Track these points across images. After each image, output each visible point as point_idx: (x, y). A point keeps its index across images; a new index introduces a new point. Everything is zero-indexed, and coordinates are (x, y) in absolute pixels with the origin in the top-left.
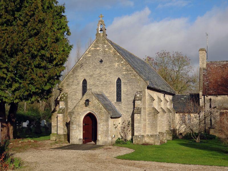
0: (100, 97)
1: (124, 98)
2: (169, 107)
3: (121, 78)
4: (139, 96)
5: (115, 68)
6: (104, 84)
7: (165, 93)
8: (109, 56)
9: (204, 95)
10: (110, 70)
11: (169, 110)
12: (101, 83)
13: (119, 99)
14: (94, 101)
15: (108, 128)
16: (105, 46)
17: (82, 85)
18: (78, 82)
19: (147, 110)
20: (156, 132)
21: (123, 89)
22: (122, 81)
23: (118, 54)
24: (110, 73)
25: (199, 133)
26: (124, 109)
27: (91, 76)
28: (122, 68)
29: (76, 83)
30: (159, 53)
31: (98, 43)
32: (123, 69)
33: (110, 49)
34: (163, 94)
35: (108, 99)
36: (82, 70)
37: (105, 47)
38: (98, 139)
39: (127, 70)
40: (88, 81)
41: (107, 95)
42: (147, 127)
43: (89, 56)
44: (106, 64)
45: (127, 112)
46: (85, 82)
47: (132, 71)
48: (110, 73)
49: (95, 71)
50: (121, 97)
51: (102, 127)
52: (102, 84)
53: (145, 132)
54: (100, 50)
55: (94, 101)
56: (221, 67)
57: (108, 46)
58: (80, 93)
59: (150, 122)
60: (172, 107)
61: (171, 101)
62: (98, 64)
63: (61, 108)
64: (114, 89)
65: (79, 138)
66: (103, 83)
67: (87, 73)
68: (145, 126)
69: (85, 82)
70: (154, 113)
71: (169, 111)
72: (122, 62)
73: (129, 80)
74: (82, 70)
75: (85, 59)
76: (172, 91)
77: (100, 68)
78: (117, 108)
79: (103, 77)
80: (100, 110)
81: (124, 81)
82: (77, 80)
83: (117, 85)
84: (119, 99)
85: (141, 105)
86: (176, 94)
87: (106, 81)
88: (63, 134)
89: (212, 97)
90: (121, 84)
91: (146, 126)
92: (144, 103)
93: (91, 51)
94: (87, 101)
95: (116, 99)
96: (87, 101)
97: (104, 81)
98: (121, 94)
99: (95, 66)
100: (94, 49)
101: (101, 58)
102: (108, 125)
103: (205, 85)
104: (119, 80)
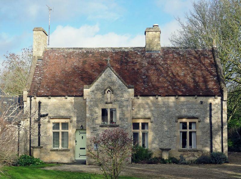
89: (43, 100)
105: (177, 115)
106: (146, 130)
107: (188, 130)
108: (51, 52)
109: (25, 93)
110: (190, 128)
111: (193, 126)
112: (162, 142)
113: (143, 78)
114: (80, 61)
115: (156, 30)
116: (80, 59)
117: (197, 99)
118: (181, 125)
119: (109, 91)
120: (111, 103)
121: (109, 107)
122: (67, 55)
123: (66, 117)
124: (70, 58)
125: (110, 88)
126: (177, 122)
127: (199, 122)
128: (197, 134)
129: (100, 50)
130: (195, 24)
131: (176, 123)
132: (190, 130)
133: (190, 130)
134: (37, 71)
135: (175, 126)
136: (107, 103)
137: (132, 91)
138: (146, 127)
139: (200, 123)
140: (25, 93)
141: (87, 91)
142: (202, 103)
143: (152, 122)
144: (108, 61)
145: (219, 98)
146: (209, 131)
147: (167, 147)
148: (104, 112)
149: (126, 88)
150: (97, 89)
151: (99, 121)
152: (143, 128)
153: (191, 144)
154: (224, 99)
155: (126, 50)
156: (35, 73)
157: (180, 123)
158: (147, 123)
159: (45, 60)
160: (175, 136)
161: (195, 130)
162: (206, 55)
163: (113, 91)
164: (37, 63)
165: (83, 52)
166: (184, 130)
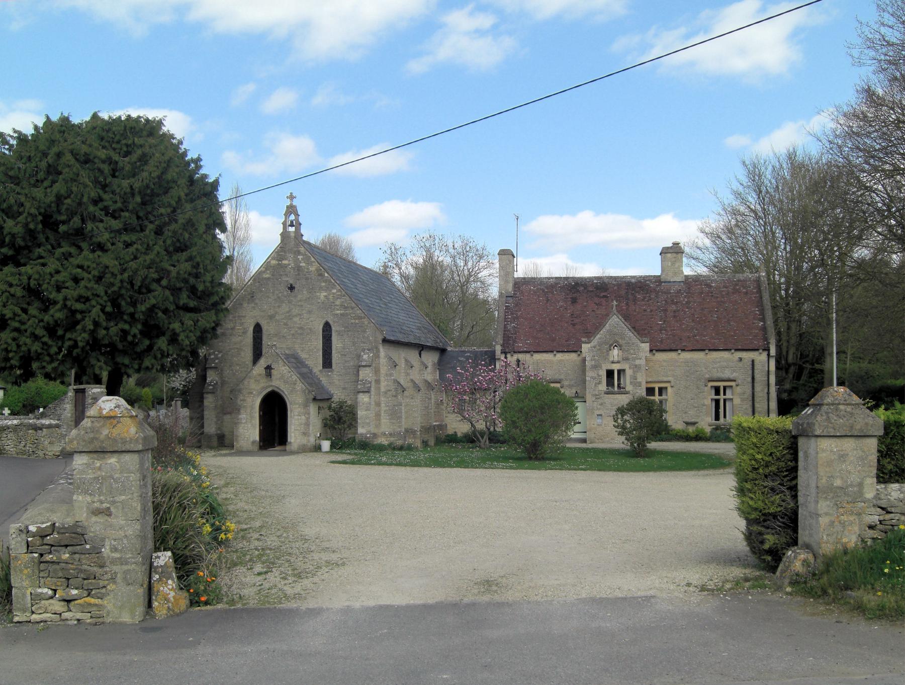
0: (295, 361)
1: (337, 362)
2: (429, 378)
3: (331, 323)
4: (367, 359)
5: (319, 303)
6: (298, 334)
7: (421, 348)
8: (307, 279)
9: (504, 352)
10: (309, 306)
11: (429, 383)
12: (292, 332)
13: (327, 362)
14: (282, 370)
15: (308, 419)
16: (300, 257)
17: (252, 336)
18: (244, 329)
19: (383, 385)
20: (400, 427)
21: (336, 343)
22: (333, 328)
23: (326, 275)
24: (310, 312)
25: (852, 552)
26: (337, 382)
27: (271, 317)
28: (334, 303)
29: (239, 331)
30: (417, 237)
31: (285, 252)
32: (336, 305)
33: (309, 263)
34: (417, 353)
35: (306, 363)
36: (253, 305)
37: (300, 259)
38: (289, 440)
39: (346, 308)
40: (265, 328)
41: (303, 355)
42: (382, 418)
43: (267, 276)
44: (302, 294)
45: (344, 389)
46: (258, 329)
47: (353, 308)
48: (310, 312)
49: (279, 307)
50: (331, 360)
51: (296, 417)
52: (293, 335)
53: (378, 426)
54: (289, 265)
55: (282, 370)
56: (543, 291)
57: (307, 259)
58: (249, 352)
59: (387, 408)
60: (438, 377)
61: (434, 364)
62: (285, 293)
63: (211, 382)
64: (319, 343)
65: (252, 440)
66: (297, 331)
67: (262, 311)
68: (378, 415)
69: (258, 329)
70: (396, 390)
71: (429, 386)
72: (334, 291)
73: (346, 327)
74: (253, 305)
75: (259, 282)
76: (441, 342)
77: (290, 302)
78: (324, 380)
79: (296, 319)
80: (292, 386)
81: (338, 328)
82: (242, 324)
83: (324, 337)
84: (327, 362)
85: (370, 375)
86: (449, 349)
87: (301, 328)
88: (215, 433)
89: (521, 356)
90: (331, 335)
91: (380, 415)
92: (377, 371)
93: (271, 267)
94: (269, 368)
95: (321, 362)
96: (269, 368)
97: (298, 328)
98: (331, 353)
99: (279, 297)
100: (277, 262)
101: (291, 282)
102: (309, 414)
103: (508, 331)
104: (327, 328)
105: (707, 376)
106: (664, 397)
107: (721, 397)
108: (523, 285)
109: (498, 349)
110: (725, 394)
111: (728, 391)
112: (686, 413)
113: (659, 324)
114: (567, 298)
115: (676, 251)
116: (567, 295)
117: (734, 355)
118: (713, 391)
119: (616, 346)
120: (618, 362)
121: (616, 367)
122: (547, 289)
123: (554, 380)
124: (552, 293)
125: (616, 342)
126: (706, 386)
127: (737, 385)
128: (734, 403)
129: (595, 281)
130: (744, 201)
131: (706, 388)
132: (725, 397)
133: (725, 397)
134: (508, 315)
135: (703, 392)
136: (613, 362)
137: (646, 347)
138: (664, 392)
139: (738, 388)
140: (498, 349)
141: (585, 347)
142: (741, 359)
143: (672, 387)
144: (614, 306)
145: (765, 353)
146: (751, 398)
147: (693, 420)
148: (610, 374)
149: (639, 341)
150: (600, 344)
151: (603, 387)
152: (660, 394)
153: (725, 416)
154: (771, 354)
155: (633, 281)
156: (505, 318)
157: (712, 387)
158: (666, 388)
159: (517, 297)
160: (704, 405)
161: (731, 397)
162: (750, 287)
163: (621, 346)
164: (506, 303)
165: (571, 284)
166: (717, 397)
